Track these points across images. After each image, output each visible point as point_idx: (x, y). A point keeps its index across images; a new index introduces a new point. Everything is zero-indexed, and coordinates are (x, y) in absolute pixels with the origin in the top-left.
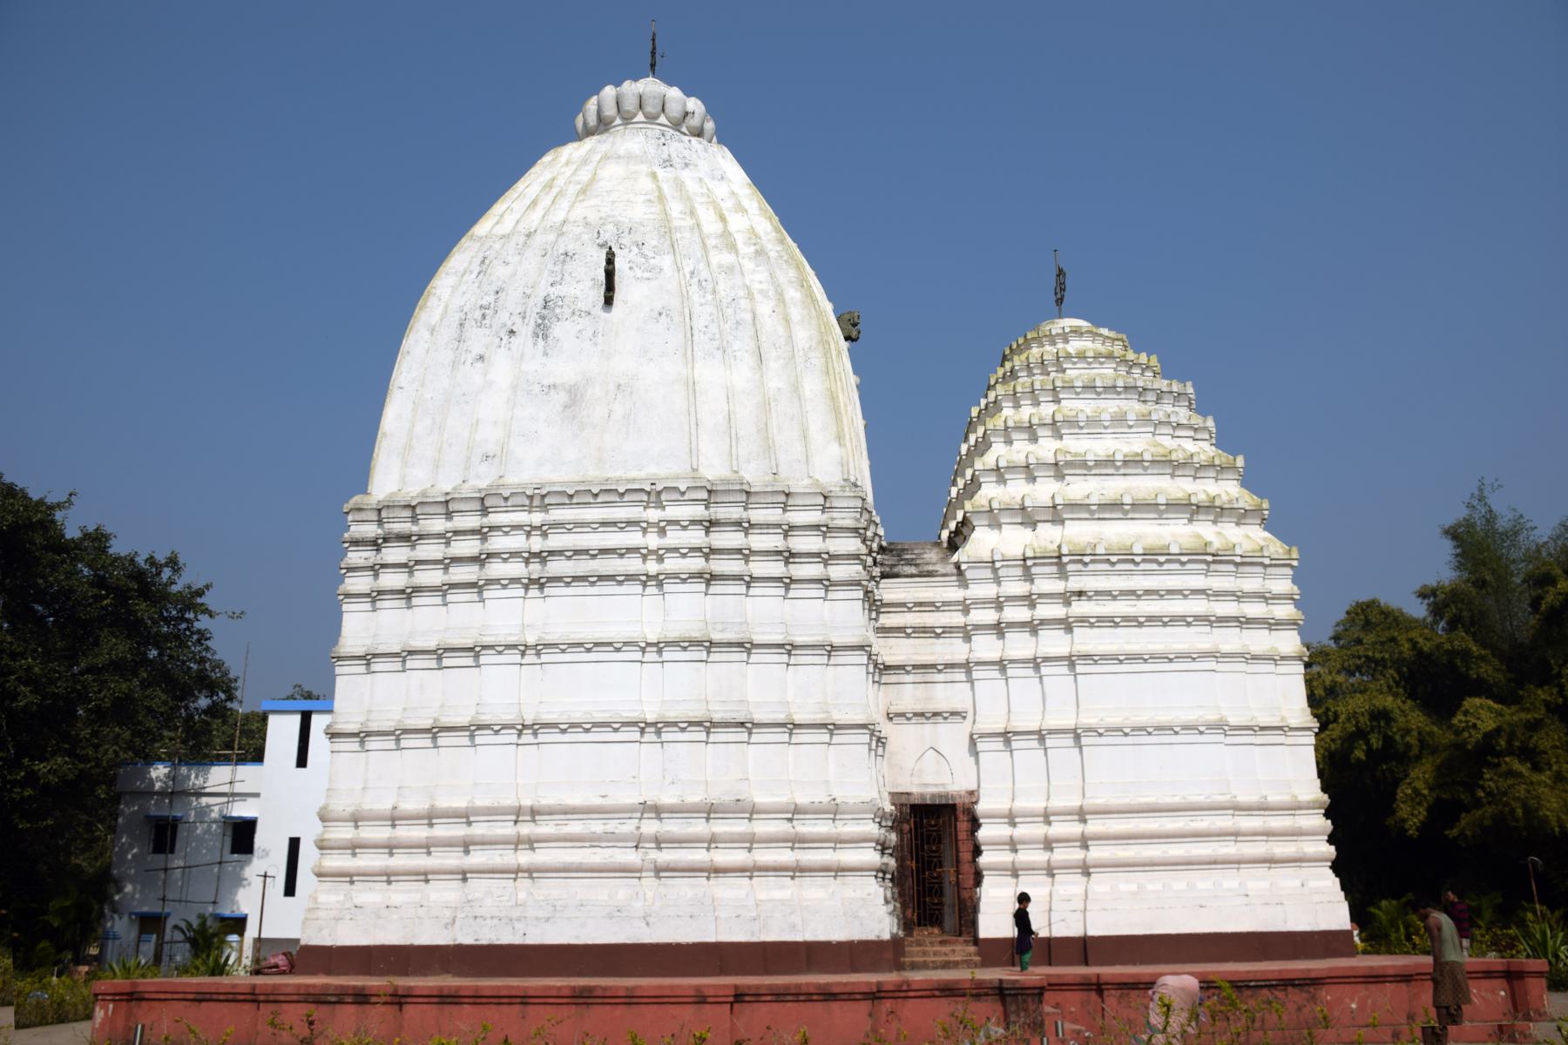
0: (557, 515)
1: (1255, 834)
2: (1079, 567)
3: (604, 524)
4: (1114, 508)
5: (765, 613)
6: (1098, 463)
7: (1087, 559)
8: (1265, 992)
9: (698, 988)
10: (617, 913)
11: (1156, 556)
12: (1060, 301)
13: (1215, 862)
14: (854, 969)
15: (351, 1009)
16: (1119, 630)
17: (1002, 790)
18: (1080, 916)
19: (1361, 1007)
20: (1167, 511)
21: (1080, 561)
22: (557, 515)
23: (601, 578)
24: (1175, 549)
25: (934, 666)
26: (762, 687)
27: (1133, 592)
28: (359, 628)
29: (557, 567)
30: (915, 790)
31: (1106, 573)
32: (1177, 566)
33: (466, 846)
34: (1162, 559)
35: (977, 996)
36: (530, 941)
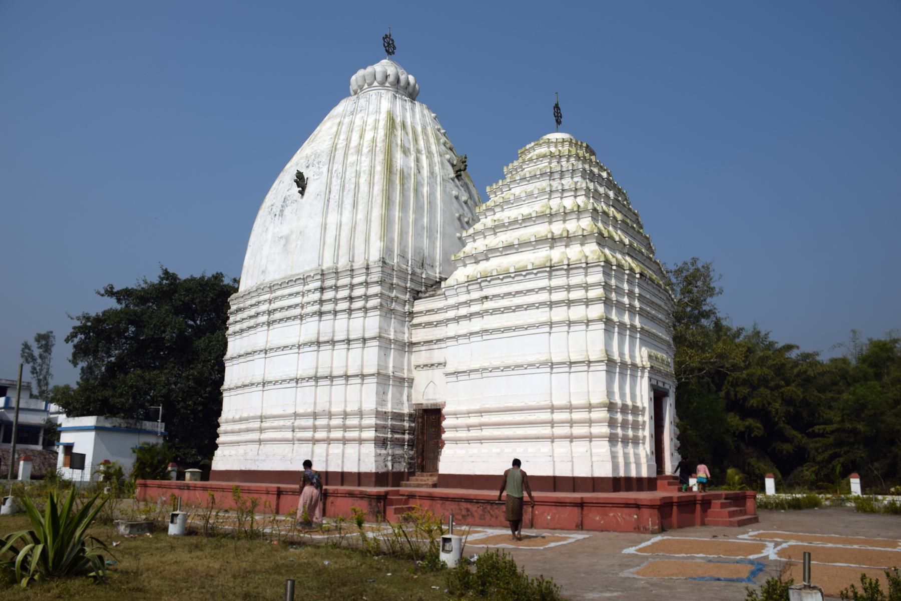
0: (279, 293)
2: (487, 283)
4: (509, 248)
5: (340, 326)
6: (510, 223)
7: (489, 279)
10: (283, 458)
11: (521, 272)
12: (559, 122)
13: (538, 438)
14: (228, 480)
16: (505, 315)
18: (570, 464)
19: (553, 519)
20: (537, 245)
21: (486, 281)
22: (279, 293)
24: (530, 267)
25: (432, 341)
27: (510, 294)
28: (235, 346)
29: (278, 315)
30: (424, 402)
31: (499, 285)
32: (533, 276)
34: (524, 273)
35: (361, 498)
36: (260, 469)
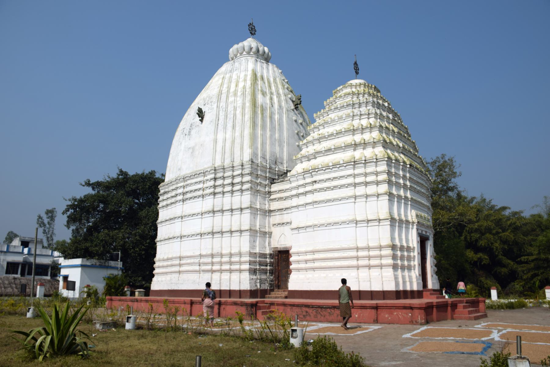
0: (189, 182)
1: (364, 257)
2: (315, 173)
3: (196, 183)
5: (227, 201)
6: (329, 136)
7: (316, 170)
8: (328, 309)
9: (184, 300)
11: (336, 166)
13: (349, 267)
15: (136, 303)
17: (297, 244)
19: (359, 317)
22: (189, 182)
23: (195, 197)
24: (341, 162)
25: (282, 209)
26: (225, 222)
27: (330, 179)
28: (163, 214)
30: (279, 246)
32: (343, 168)
33: (180, 265)
34: (338, 166)
36: (180, 289)
